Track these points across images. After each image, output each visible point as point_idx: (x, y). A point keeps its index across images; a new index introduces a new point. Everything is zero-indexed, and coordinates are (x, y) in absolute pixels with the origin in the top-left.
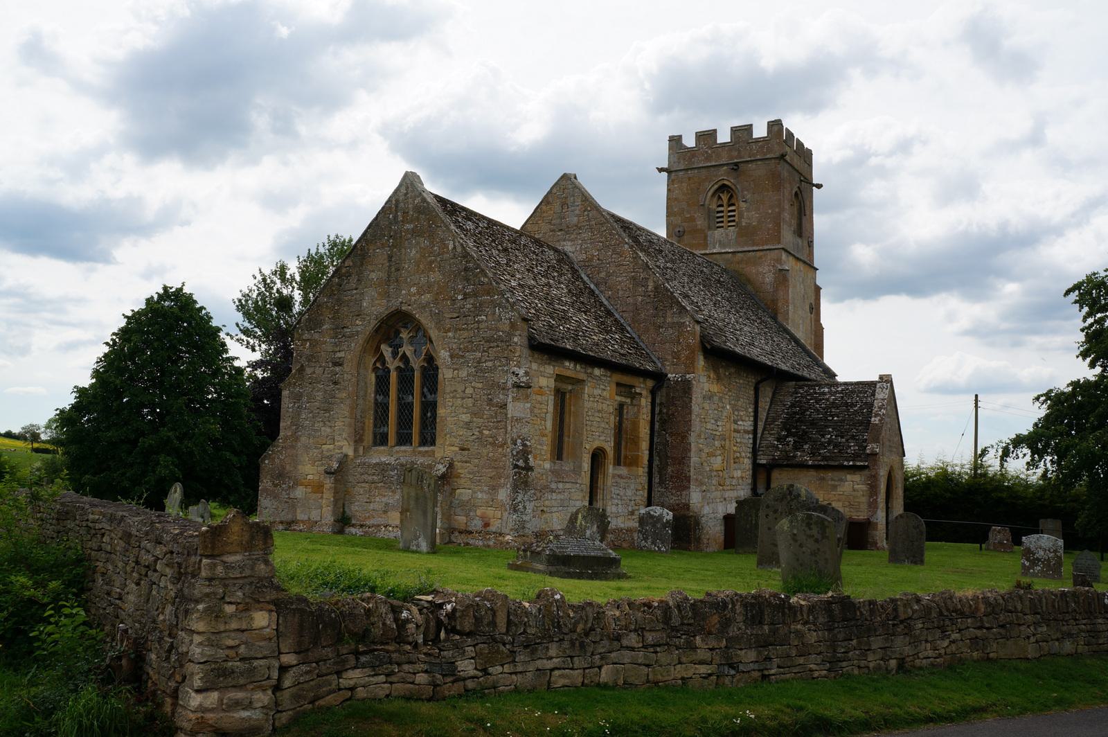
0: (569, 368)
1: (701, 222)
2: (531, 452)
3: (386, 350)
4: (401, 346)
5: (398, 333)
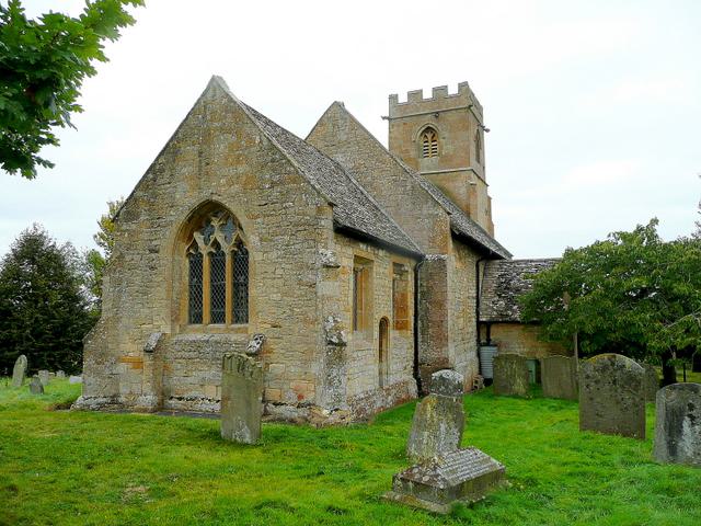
0: (363, 250)
1: (413, 154)
2: (343, 328)
3: (198, 237)
4: (212, 233)
5: (209, 221)
